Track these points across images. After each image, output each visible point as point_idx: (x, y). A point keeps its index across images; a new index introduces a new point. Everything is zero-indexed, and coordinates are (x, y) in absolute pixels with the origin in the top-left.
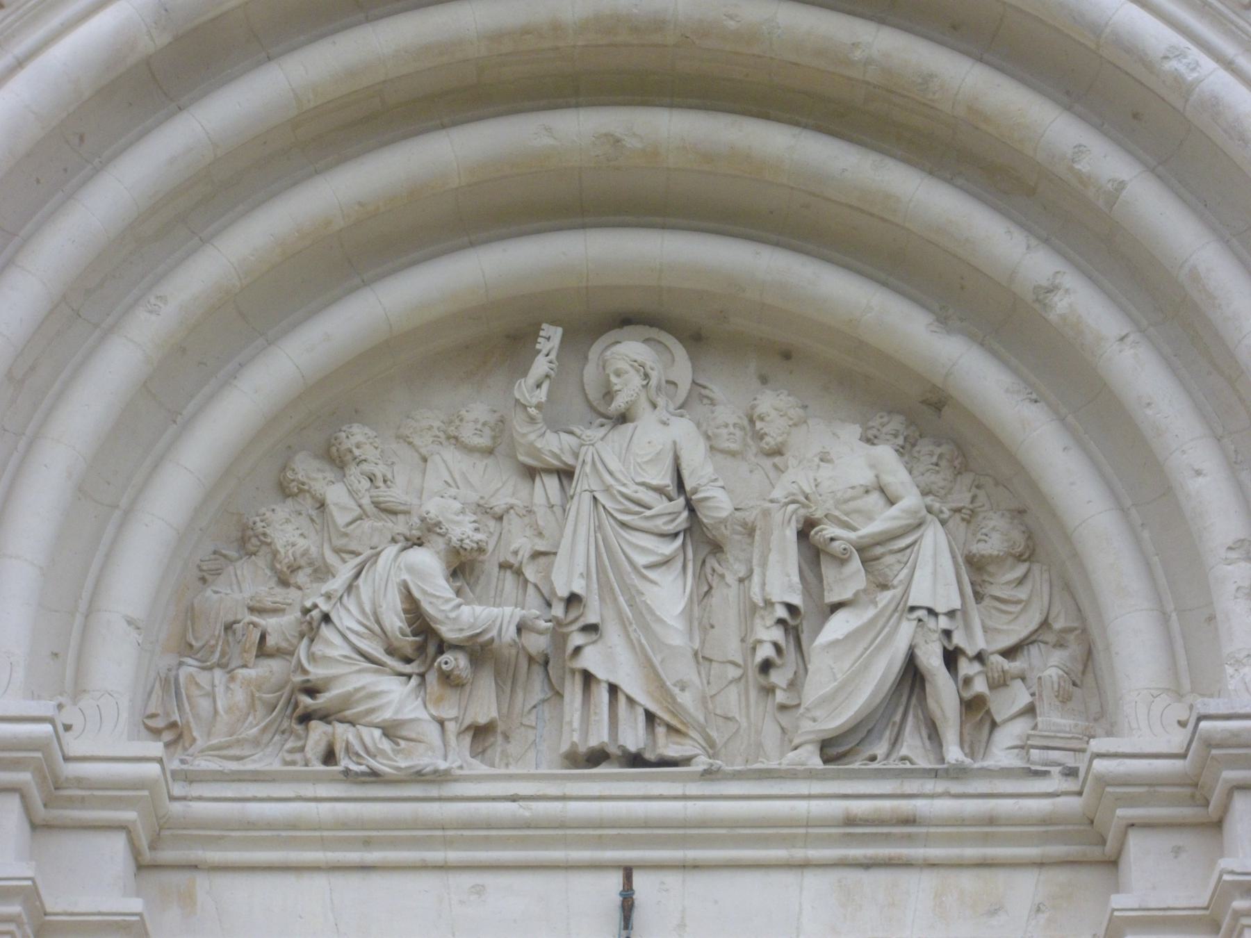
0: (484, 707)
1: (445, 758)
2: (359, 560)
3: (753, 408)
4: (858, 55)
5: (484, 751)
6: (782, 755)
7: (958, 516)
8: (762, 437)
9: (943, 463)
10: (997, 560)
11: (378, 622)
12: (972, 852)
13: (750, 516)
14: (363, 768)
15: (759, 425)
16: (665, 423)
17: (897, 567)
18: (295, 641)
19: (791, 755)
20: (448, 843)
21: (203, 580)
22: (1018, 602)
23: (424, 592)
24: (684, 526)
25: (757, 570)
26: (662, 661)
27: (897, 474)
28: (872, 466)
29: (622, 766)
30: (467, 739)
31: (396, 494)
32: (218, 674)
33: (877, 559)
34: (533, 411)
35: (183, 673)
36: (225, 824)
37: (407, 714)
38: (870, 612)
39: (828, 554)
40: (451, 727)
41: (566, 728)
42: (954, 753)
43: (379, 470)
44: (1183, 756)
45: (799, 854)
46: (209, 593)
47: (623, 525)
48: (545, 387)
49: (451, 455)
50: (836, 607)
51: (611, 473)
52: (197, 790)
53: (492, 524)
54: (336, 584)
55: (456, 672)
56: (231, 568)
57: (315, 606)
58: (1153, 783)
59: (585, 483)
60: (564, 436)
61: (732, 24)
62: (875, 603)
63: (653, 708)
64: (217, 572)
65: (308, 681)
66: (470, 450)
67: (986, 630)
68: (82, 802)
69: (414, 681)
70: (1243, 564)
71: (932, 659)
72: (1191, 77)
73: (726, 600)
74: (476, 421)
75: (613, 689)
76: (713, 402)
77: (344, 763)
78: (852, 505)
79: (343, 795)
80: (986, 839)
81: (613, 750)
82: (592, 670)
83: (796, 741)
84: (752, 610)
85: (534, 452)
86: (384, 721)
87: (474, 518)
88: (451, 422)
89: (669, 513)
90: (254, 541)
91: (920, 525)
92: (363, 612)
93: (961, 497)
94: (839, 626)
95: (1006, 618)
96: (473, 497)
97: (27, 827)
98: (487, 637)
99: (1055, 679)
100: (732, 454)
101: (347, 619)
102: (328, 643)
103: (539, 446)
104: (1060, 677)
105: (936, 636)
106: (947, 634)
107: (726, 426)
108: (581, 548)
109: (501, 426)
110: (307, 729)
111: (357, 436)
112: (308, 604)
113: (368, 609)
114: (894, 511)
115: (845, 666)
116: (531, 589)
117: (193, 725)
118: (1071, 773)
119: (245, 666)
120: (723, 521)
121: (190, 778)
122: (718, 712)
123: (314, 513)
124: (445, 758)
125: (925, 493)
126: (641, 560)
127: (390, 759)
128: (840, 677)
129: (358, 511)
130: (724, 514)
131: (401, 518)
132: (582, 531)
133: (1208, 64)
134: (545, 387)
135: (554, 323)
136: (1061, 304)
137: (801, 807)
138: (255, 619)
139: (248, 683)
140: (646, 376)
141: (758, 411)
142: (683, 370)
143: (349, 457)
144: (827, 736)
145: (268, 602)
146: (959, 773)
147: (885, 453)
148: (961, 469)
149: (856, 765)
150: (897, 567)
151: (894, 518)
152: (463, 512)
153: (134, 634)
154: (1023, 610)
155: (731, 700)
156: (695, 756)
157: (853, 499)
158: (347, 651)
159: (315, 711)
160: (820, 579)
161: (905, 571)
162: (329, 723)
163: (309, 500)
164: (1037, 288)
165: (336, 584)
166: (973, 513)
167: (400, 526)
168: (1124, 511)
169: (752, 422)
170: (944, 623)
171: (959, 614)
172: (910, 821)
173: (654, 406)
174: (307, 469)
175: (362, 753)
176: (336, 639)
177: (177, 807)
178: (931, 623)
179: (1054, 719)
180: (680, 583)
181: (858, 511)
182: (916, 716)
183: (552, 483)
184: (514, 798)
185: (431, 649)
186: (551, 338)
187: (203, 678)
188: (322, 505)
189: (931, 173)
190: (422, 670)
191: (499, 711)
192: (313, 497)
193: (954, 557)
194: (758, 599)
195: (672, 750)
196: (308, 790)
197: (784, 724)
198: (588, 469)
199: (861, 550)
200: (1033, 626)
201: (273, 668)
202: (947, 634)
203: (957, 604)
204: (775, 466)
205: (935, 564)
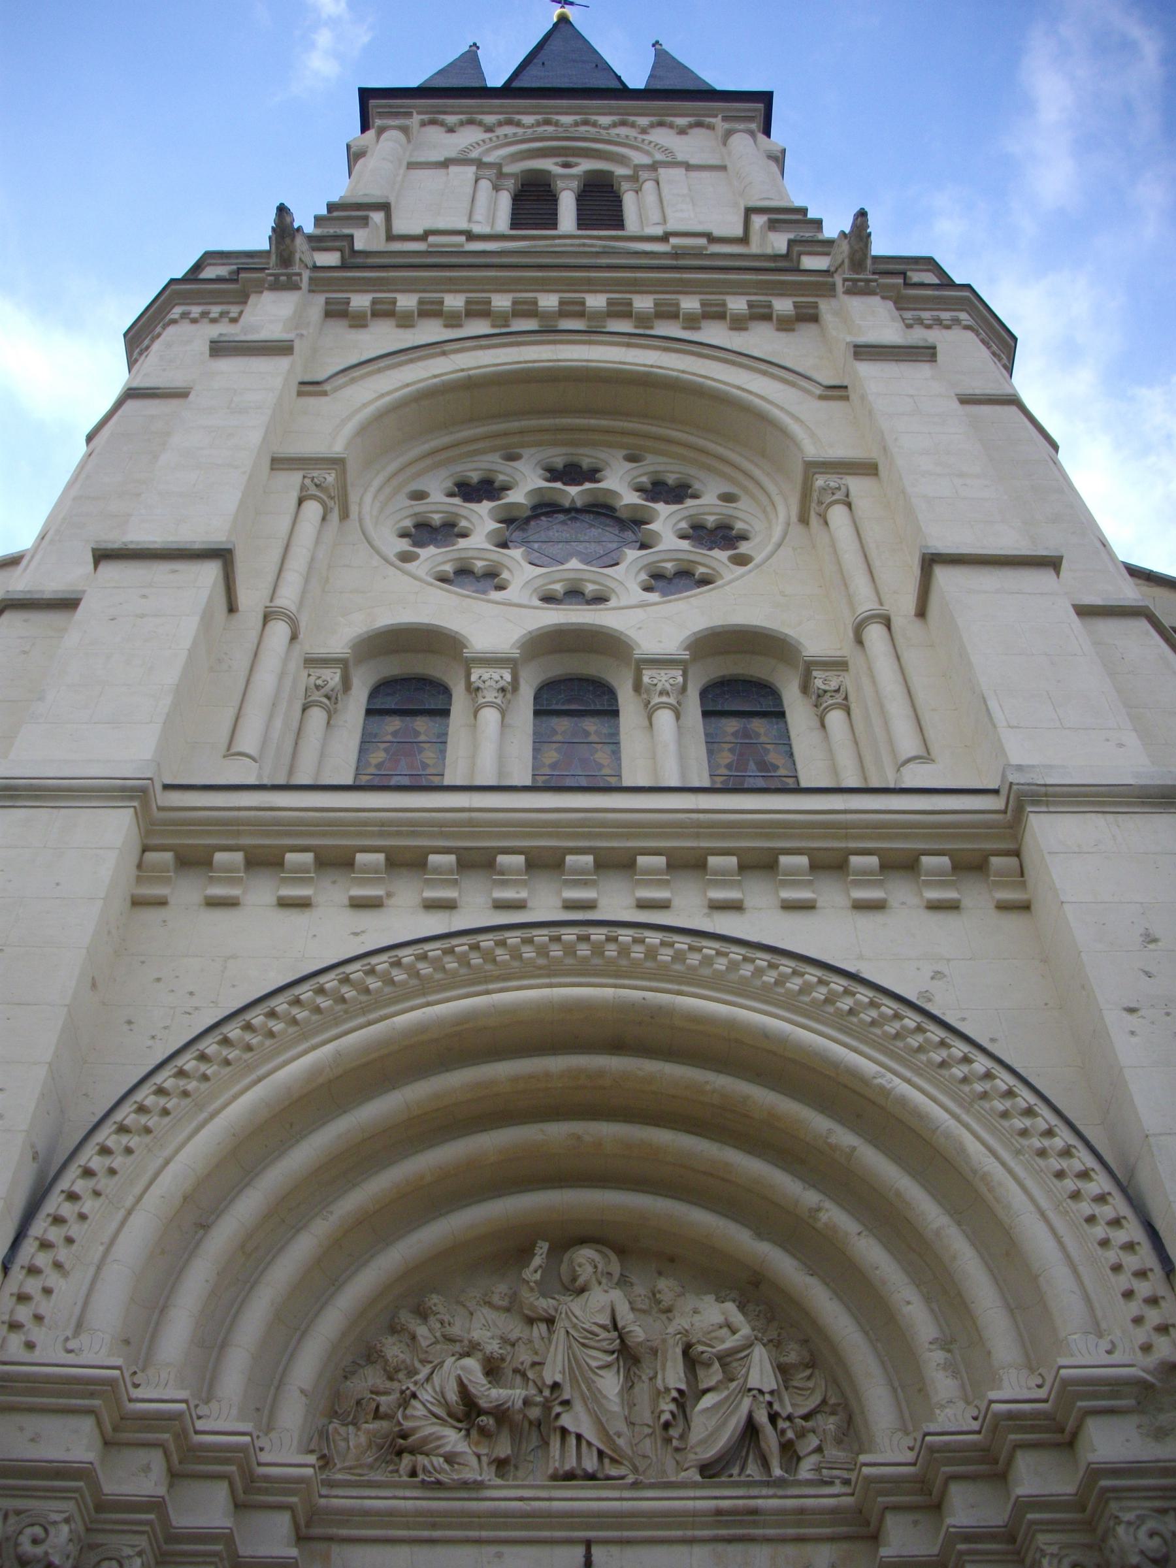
0: (504, 1449)
1: (481, 1475)
3: (654, 1287)
4: (708, 1087)
6: (677, 1474)
9: (761, 1315)
10: (793, 1366)
11: (444, 1397)
12: (791, 1531)
13: (654, 1344)
14: (433, 1479)
15: (658, 1296)
16: (606, 1291)
17: (739, 1368)
19: (683, 1474)
20: (481, 1527)
22: (809, 1389)
23: (470, 1381)
24: (618, 1347)
26: (607, 1420)
27: (737, 1318)
28: (723, 1314)
30: (493, 1468)
31: (456, 1330)
32: (351, 1428)
34: (532, 1284)
35: (331, 1427)
36: (351, 1512)
38: (726, 1393)
39: (699, 1362)
40: (484, 1459)
41: (551, 1461)
42: (777, 1472)
43: (447, 1318)
44: (914, 1464)
45: (689, 1533)
46: (348, 1383)
47: (583, 1345)
48: (539, 1272)
49: (486, 1310)
50: (705, 1391)
51: (576, 1317)
52: (335, 1492)
53: (509, 1348)
54: (421, 1377)
55: (488, 1427)
56: (361, 1370)
57: (408, 1388)
58: (897, 1481)
59: (561, 1325)
62: (727, 1388)
63: (602, 1447)
64: (353, 1373)
65: (402, 1430)
66: (496, 1308)
67: (793, 1405)
68: (267, 1492)
69: (463, 1432)
70: (939, 1351)
71: (762, 1417)
72: (889, 1086)
73: (642, 1390)
74: (501, 1293)
75: (579, 1437)
76: (632, 1284)
77: (421, 1476)
78: (713, 1335)
80: (799, 1524)
81: (579, 1472)
83: (686, 1466)
84: (658, 1394)
85: (533, 1307)
86: (445, 1452)
88: (486, 1295)
89: (608, 1339)
90: (375, 1355)
91: (751, 1345)
92: (435, 1391)
93: (773, 1334)
94: (708, 1401)
95: (800, 1398)
96: (499, 1333)
97: (231, 1506)
98: (506, 1406)
99: (833, 1429)
101: (426, 1395)
102: (415, 1408)
105: (764, 1405)
107: (640, 1296)
108: (560, 1357)
109: (514, 1297)
110: (401, 1460)
111: (434, 1300)
112: (404, 1388)
113: (438, 1389)
114: (736, 1336)
115: (712, 1423)
116: (531, 1383)
117: (335, 1456)
118: (846, 1482)
119: (366, 1422)
120: (640, 1344)
121: (331, 1484)
122: (639, 1453)
123: (409, 1341)
124: (481, 1475)
125: (753, 1330)
126: (594, 1364)
127: (447, 1474)
128: (710, 1429)
130: (640, 1340)
131: (458, 1344)
132: (561, 1348)
133: (897, 1081)
134: (539, 1272)
135: (544, 1240)
136: (824, 1217)
137: (690, 1503)
138: (374, 1396)
139: (368, 1432)
140: (596, 1267)
142: (615, 1268)
143: (429, 1311)
144: (705, 1462)
145: (381, 1388)
147: (730, 1307)
148: (770, 1320)
149: (723, 1479)
150: (739, 1368)
151: (738, 1340)
152: (492, 1338)
153: (304, 1398)
154: (811, 1393)
155: (647, 1446)
156: (627, 1475)
158: (425, 1412)
159: (406, 1448)
161: (744, 1370)
162: (414, 1455)
164: (810, 1210)
165: (421, 1377)
167: (457, 1348)
168: (866, 1333)
169: (654, 1295)
170: (768, 1397)
171: (776, 1394)
172: (754, 1512)
173: (600, 1283)
174: (406, 1318)
175: (432, 1471)
177: (323, 1501)
178: (761, 1398)
179: (833, 1453)
180: (616, 1377)
181: (716, 1338)
182: (755, 1454)
183: (543, 1327)
185: (474, 1415)
186: (542, 1248)
187: (342, 1430)
188: (414, 1338)
189: (749, 1153)
190: (467, 1427)
193: (771, 1364)
194: (661, 1387)
195: (613, 1472)
196: (400, 1493)
197: (677, 1458)
198: (563, 1316)
199: (720, 1359)
200: (818, 1402)
201: (384, 1425)
202: (770, 1404)
203: (776, 1388)
205: (761, 1364)
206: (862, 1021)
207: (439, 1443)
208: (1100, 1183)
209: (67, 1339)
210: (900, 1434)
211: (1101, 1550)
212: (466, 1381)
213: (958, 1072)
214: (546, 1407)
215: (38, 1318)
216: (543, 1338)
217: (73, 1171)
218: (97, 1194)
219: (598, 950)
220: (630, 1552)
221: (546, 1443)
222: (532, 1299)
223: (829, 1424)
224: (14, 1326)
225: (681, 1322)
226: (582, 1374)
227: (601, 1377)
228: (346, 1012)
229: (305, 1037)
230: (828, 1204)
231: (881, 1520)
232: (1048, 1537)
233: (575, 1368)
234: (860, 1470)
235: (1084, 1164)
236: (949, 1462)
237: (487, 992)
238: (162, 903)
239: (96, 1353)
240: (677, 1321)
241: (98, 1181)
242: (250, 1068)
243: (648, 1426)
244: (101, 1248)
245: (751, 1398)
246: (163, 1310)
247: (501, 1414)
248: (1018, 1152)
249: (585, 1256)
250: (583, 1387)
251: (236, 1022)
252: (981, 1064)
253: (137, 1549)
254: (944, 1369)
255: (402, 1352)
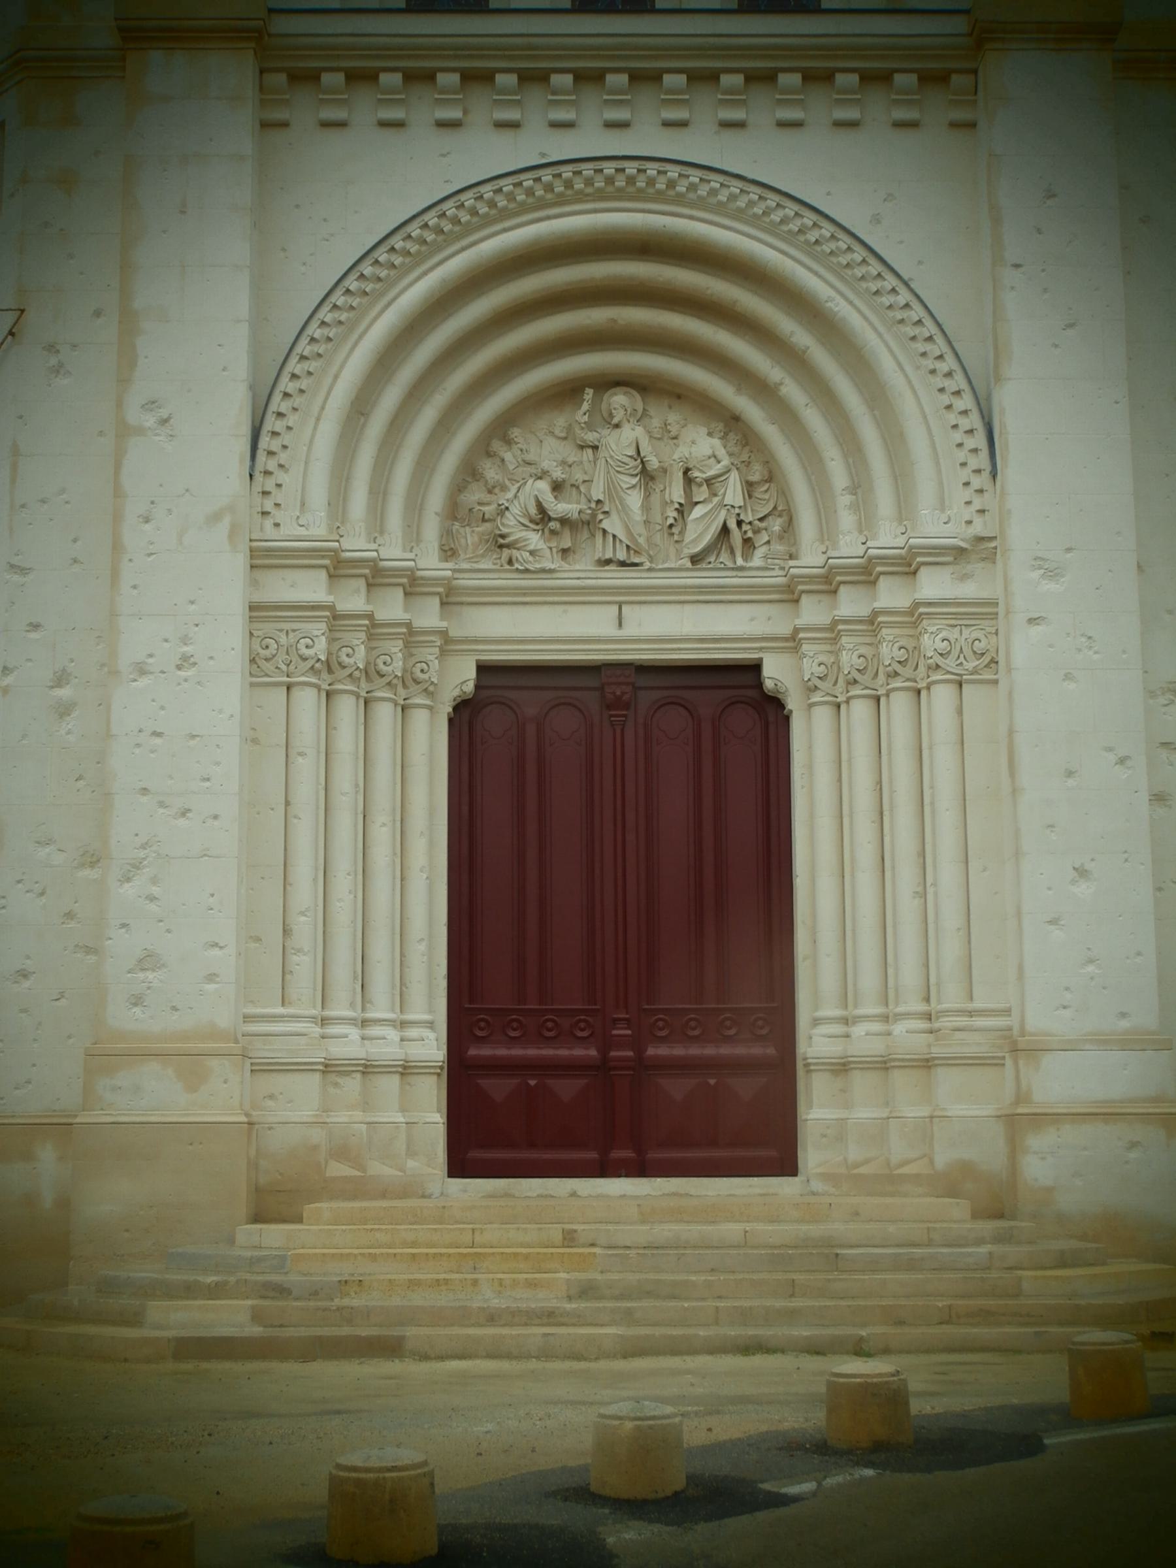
0: (567, 543)
2: (518, 485)
3: (667, 420)
4: (709, 292)
5: (566, 558)
7: (743, 464)
8: (670, 432)
9: (739, 443)
10: (758, 483)
11: (527, 510)
14: (523, 568)
15: (669, 427)
16: (633, 430)
18: (495, 516)
19: (680, 562)
21: (459, 490)
22: (765, 500)
25: (668, 488)
27: (721, 452)
28: (711, 448)
29: (617, 567)
30: (560, 554)
33: (713, 484)
34: (583, 425)
37: (539, 547)
38: (710, 506)
40: (554, 550)
41: (596, 553)
42: (740, 561)
43: (524, 447)
45: (682, 598)
47: (618, 472)
50: (697, 503)
51: (613, 451)
53: (567, 468)
54: (510, 495)
59: (602, 453)
60: (594, 433)
61: (661, 279)
63: (629, 544)
64: (465, 488)
66: (559, 438)
67: (752, 510)
68: (423, 585)
69: (540, 532)
72: (836, 309)
73: (656, 499)
75: (614, 536)
76: (651, 417)
77: (517, 566)
79: (517, 577)
82: (606, 528)
84: (665, 504)
85: (584, 441)
87: (561, 468)
91: (729, 471)
93: (745, 457)
94: (698, 511)
98: (567, 517)
100: (659, 439)
101: (515, 509)
102: (507, 518)
103: (585, 438)
104: (780, 530)
105: (734, 515)
106: (738, 515)
108: (601, 483)
109: (569, 429)
110: (501, 550)
114: (719, 466)
115: (701, 528)
116: (583, 496)
119: (477, 527)
120: (656, 470)
123: (500, 464)
126: (625, 486)
128: (699, 532)
129: (517, 464)
130: (655, 467)
133: (843, 303)
135: (590, 387)
140: (626, 410)
141: (668, 422)
142: (639, 406)
143: (512, 441)
145: (485, 500)
146: (742, 569)
147: (716, 442)
151: (719, 469)
152: (557, 466)
155: (658, 538)
157: (703, 460)
158: (516, 523)
160: (691, 491)
162: (509, 549)
163: (498, 459)
164: (775, 384)
165: (510, 495)
166: (749, 463)
169: (665, 424)
170: (737, 511)
173: (629, 422)
174: (497, 445)
176: (512, 518)
178: (732, 510)
179: (779, 548)
181: (705, 465)
183: (590, 451)
184: (578, 578)
186: (589, 393)
187: (462, 530)
188: (503, 460)
191: (572, 543)
192: (500, 457)
195: (636, 560)
198: (604, 448)
200: (770, 509)
201: (488, 525)
202: (738, 515)
203: (742, 504)
204: (675, 444)
206: (823, 251)
207: (527, 542)
208: (966, 402)
209: (298, 517)
210: (817, 543)
211: (918, 639)
212: (541, 500)
213: (886, 300)
214: (594, 516)
215: (278, 505)
216: (590, 462)
217: (277, 397)
218: (295, 409)
219: (631, 180)
220: (645, 608)
221: (593, 536)
222: (583, 435)
223: (776, 525)
224: (265, 514)
225: (682, 451)
226: (617, 493)
227: (629, 495)
228: (445, 241)
229: (418, 264)
230: (788, 381)
231: (800, 597)
232: (889, 631)
233: (612, 489)
234: (789, 570)
235: (958, 386)
236: (840, 574)
237: (548, 218)
238: (285, 125)
239: (319, 527)
240: (680, 449)
241: (295, 400)
242: (382, 294)
243: (660, 524)
244: (305, 448)
245: (726, 511)
246: (348, 479)
247: (564, 521)
248: (918, 368)
249: (619, 400)
250: (617, 502)
251: (368, 259)
252: (904, 296)
253: (361, 641)
254: (850, 509)
255: (497, 474)
